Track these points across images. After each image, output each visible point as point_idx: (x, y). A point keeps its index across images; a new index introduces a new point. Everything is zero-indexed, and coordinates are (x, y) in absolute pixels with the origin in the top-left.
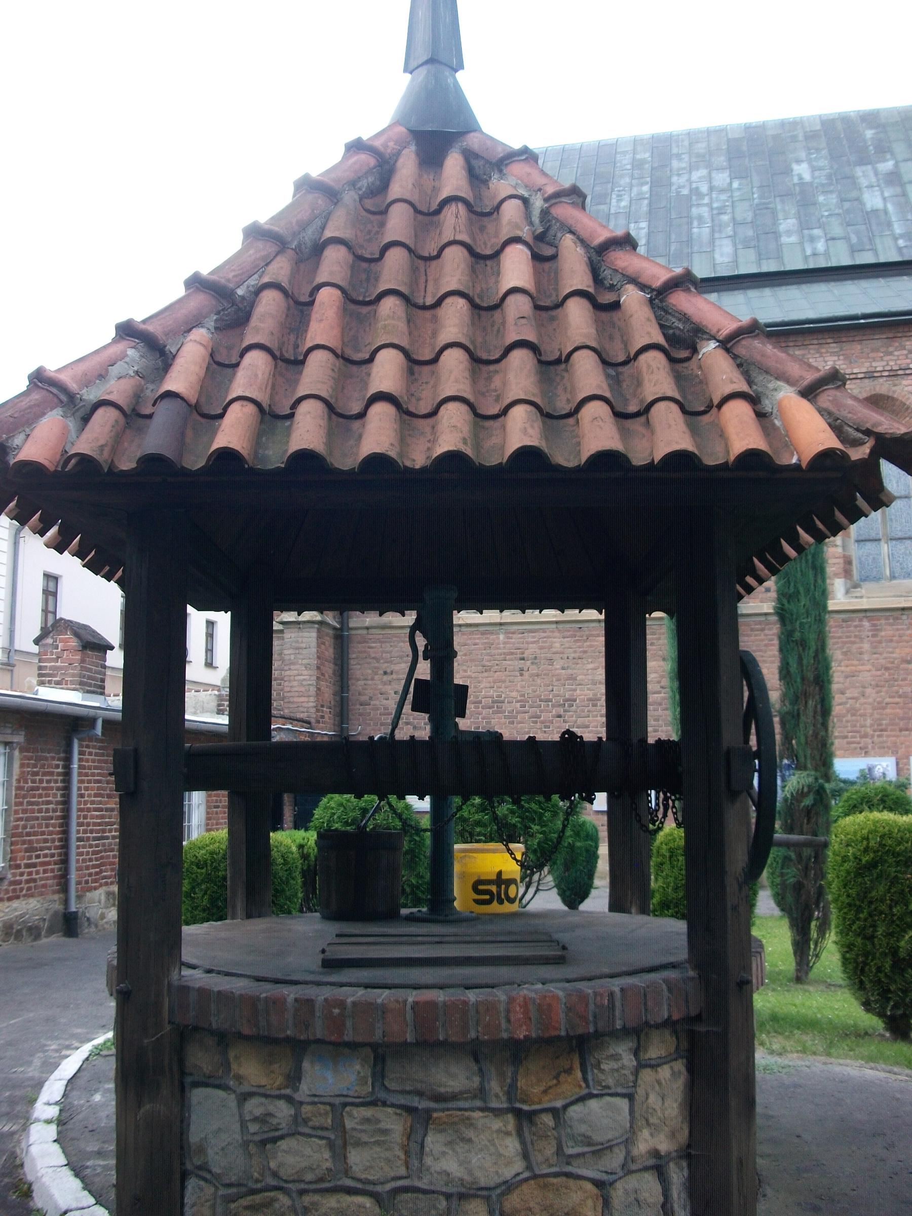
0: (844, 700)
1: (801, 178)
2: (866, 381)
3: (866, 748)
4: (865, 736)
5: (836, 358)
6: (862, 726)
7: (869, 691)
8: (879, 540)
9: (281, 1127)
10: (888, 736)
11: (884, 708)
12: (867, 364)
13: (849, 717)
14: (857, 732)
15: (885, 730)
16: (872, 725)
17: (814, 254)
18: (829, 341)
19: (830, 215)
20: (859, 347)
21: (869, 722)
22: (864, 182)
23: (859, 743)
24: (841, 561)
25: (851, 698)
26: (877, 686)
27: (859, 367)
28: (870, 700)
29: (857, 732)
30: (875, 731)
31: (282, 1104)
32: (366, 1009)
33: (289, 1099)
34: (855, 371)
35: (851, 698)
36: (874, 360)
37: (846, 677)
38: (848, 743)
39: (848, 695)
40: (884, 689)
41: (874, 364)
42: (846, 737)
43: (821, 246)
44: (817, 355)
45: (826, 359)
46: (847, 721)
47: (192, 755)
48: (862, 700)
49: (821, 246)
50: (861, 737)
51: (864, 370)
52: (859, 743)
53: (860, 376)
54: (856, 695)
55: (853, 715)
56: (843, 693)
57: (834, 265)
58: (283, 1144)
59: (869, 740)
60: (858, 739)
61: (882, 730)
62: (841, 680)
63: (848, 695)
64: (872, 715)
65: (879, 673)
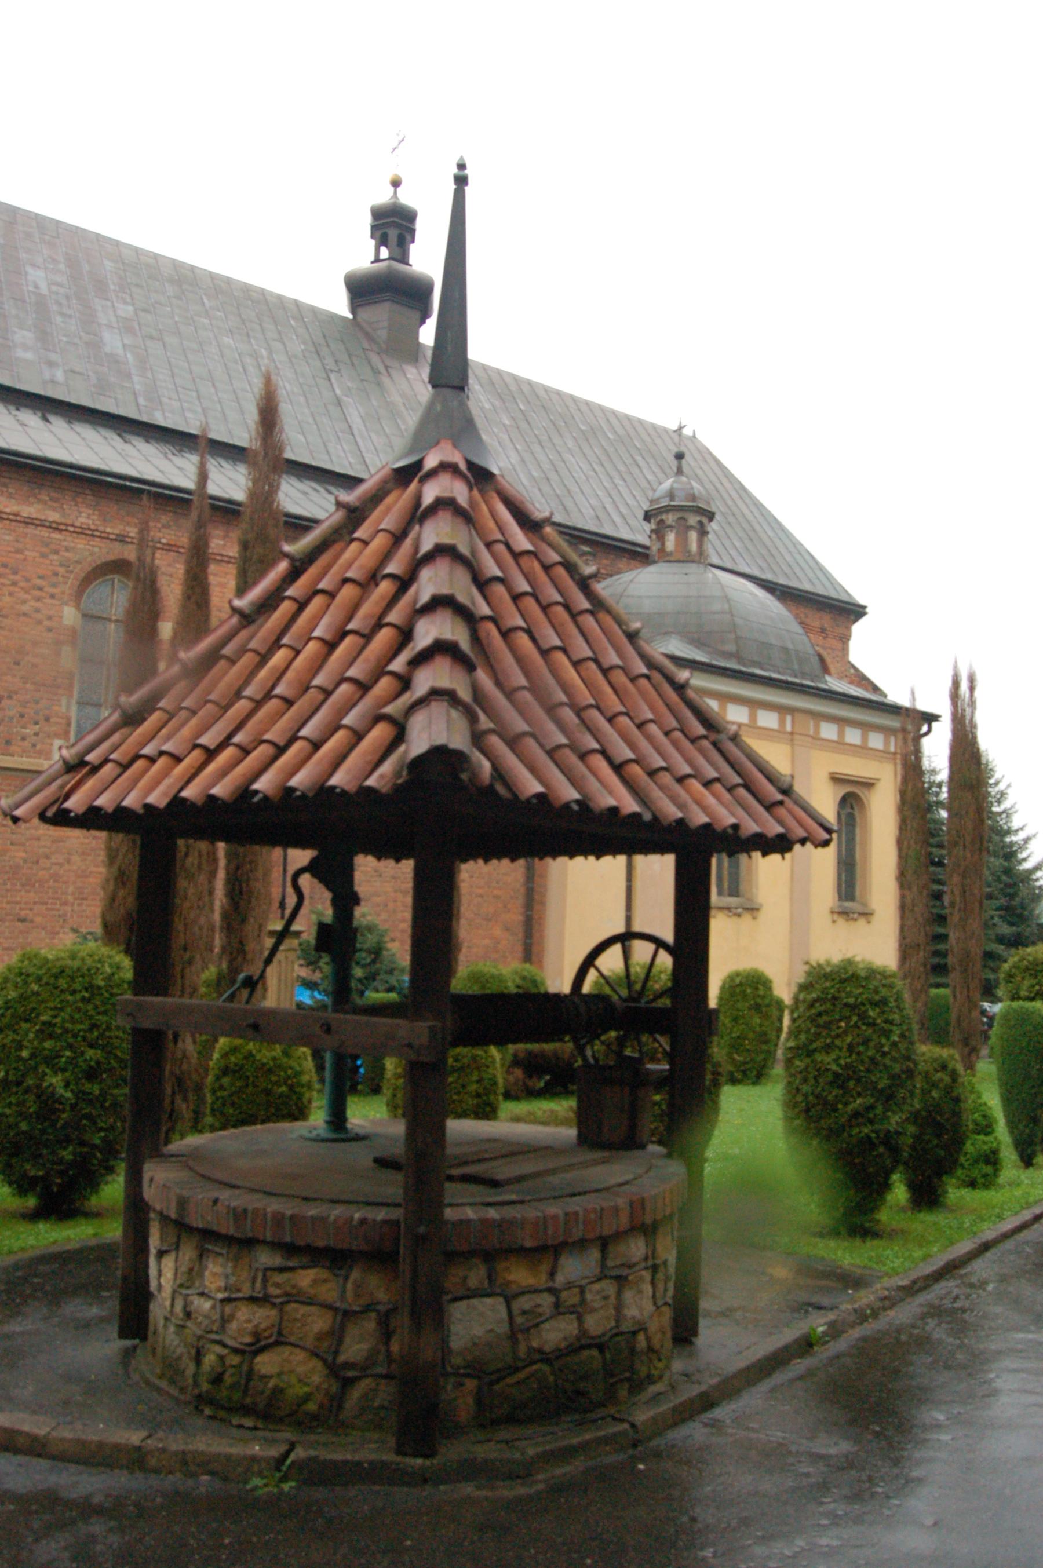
0: (48, 865)
1: (36, 287)
2: (117, 544)
3: (65, 915)
4: (66, 903)
5: (91, 512)
6: (62, 893)
7: (76, 858)
8: (100, 705)
9: (540, 1310)
10: (88, 906)
11: (87, 877)
12: (121, 527)
13: (51, 883)
14: (58, 899)
15: (86, 899)
16: (73, 894)
17: (53, 381)
18: (87, 492)
19: (68, 342)
20: (116, 507)
21: (71, 889)
22: (103, 319)
23: (58, 910)
24: (63, 721)
25: (56, 864)
26: (83, 853)
27: (112, 527)
28: (75, 868)
29: (58, 899)
30: (76, 899)
31: (545, 1295)
32: (571, 1217)
33: (550, 1290)
34: (108, 530)
35: (56, 864)
36: (128, 524)
37: (53, 842)
38: (47, 909)
39: (53, 860)
40: (90, 858)
41: (128, 529)
42: (46, 904)
43: (59, 375)
44: (73, 503)
45: (82, 510)
46: (49, 888)
47: (462, 1001)
48: (66, 867)
49: (59, 375)
50: (61, 905)
51: (117, 531)
52: (58, 910)
53: (113, 537)
54: (61, 861)
55: (56, 881)
56: (47, 857)
57: (73, 401)
58: (547, 1326)
59: (69, 909)
60: (58, 906)
61: (82, 899)
62: (48, 844)
63: (53, 860)
64: (74, 883)
65: (87, 841)
